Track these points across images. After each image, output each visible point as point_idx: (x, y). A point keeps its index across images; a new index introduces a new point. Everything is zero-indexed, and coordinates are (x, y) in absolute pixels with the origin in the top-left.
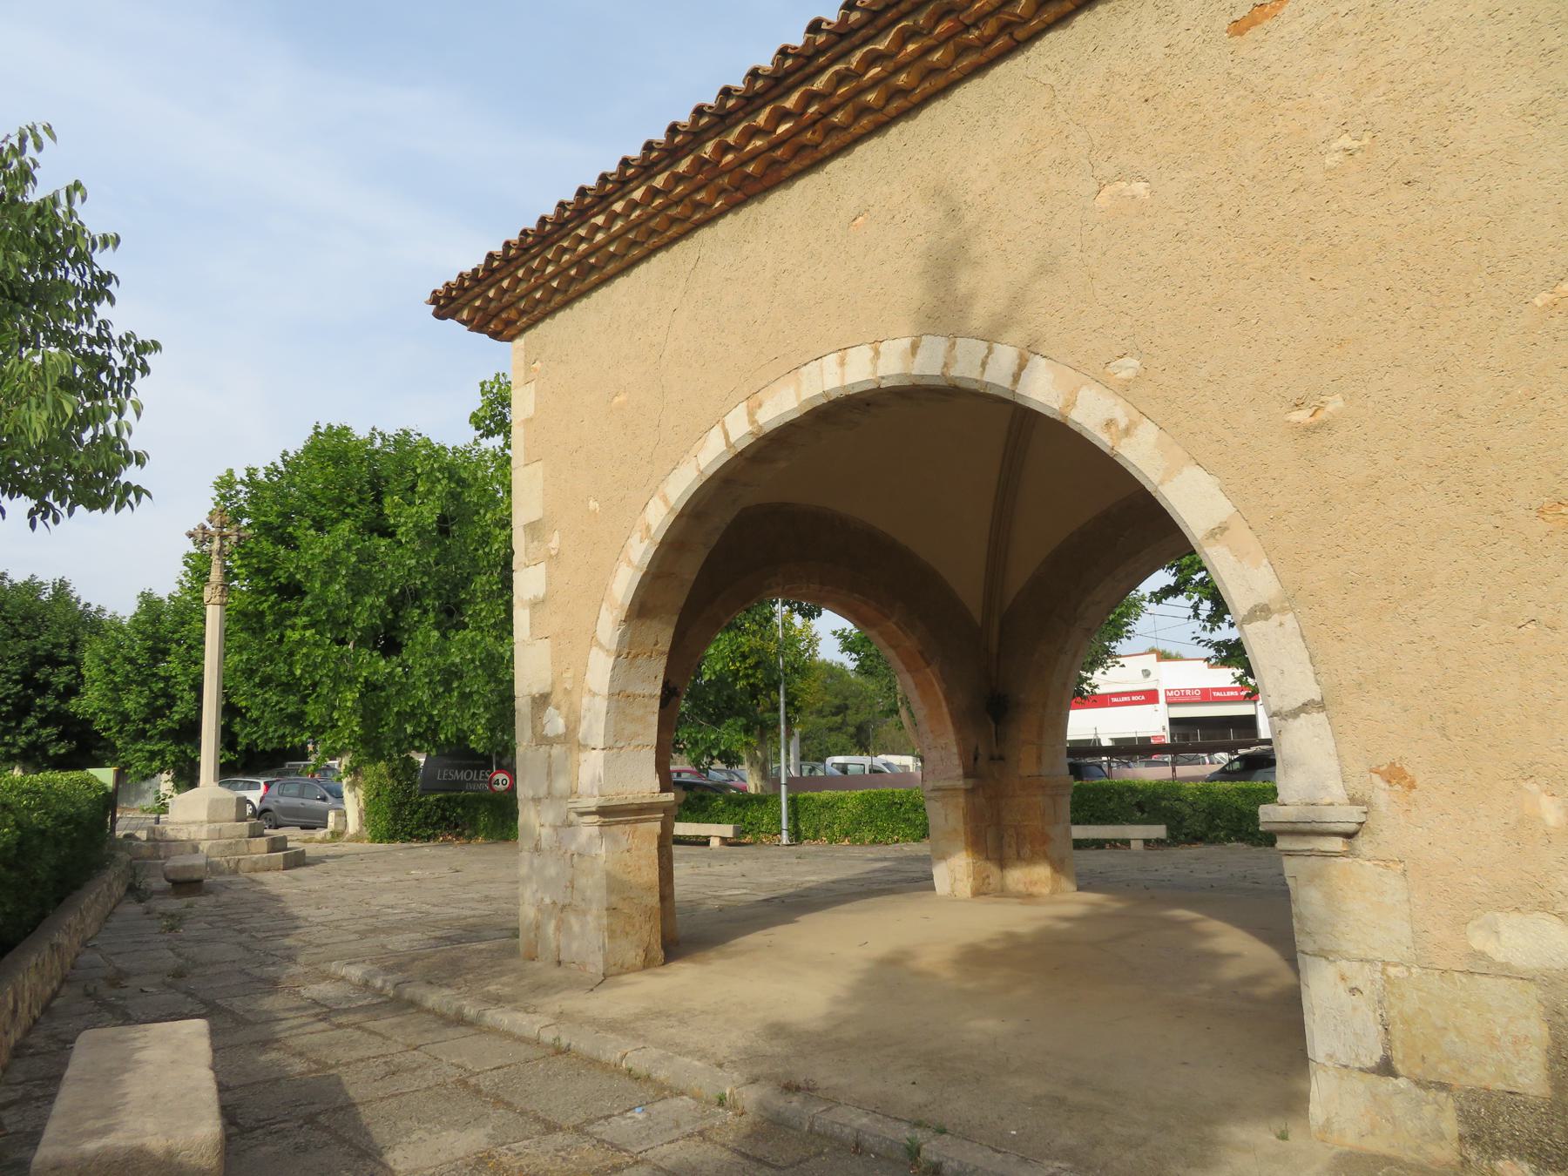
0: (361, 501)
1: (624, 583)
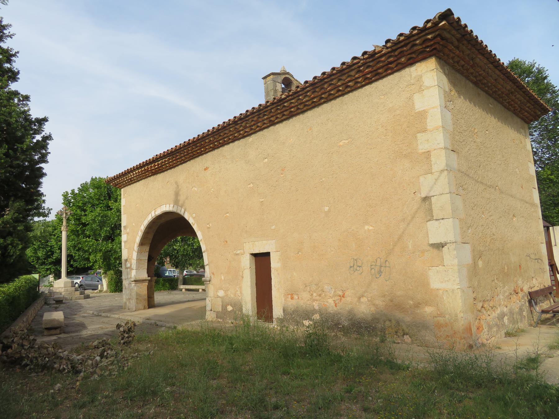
0: (105, 199)
1: (138, 240)
